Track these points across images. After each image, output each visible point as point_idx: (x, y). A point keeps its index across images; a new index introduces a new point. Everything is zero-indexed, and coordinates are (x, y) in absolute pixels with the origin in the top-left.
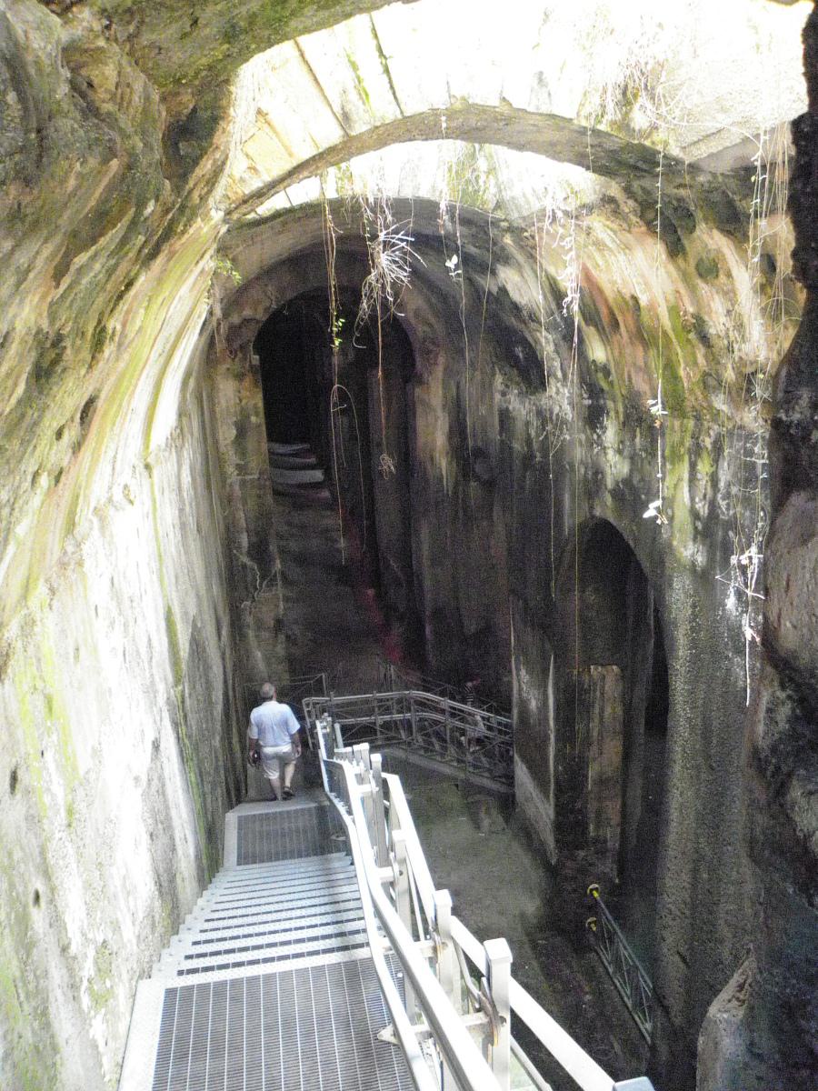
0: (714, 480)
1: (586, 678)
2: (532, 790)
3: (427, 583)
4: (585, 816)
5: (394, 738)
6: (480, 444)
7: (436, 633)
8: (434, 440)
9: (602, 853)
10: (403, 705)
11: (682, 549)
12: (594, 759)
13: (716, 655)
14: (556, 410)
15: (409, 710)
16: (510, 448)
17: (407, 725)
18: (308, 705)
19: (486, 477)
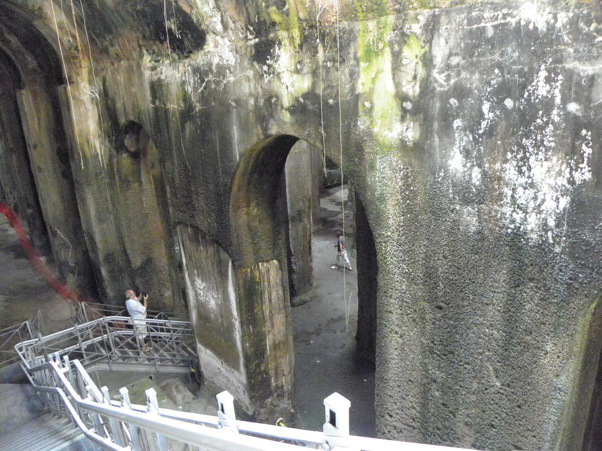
0: (427, 61)
1: (257, 274)
2: (219, 366)
3: (98, 238)
4: (267, 374)
5: (97, 356)
6: (132, 118)
7: (110, 272)
8: (88, 128)
9: (281, 396)
10: (98, 332)
11: (387, 132)
12: (269, 332)
13: (437, 213)
14: (216, 61)
15: (105, 332)
16: (166, 111)
17: (104, 344)
18: (21, 349)
19: (132, 149)
